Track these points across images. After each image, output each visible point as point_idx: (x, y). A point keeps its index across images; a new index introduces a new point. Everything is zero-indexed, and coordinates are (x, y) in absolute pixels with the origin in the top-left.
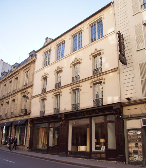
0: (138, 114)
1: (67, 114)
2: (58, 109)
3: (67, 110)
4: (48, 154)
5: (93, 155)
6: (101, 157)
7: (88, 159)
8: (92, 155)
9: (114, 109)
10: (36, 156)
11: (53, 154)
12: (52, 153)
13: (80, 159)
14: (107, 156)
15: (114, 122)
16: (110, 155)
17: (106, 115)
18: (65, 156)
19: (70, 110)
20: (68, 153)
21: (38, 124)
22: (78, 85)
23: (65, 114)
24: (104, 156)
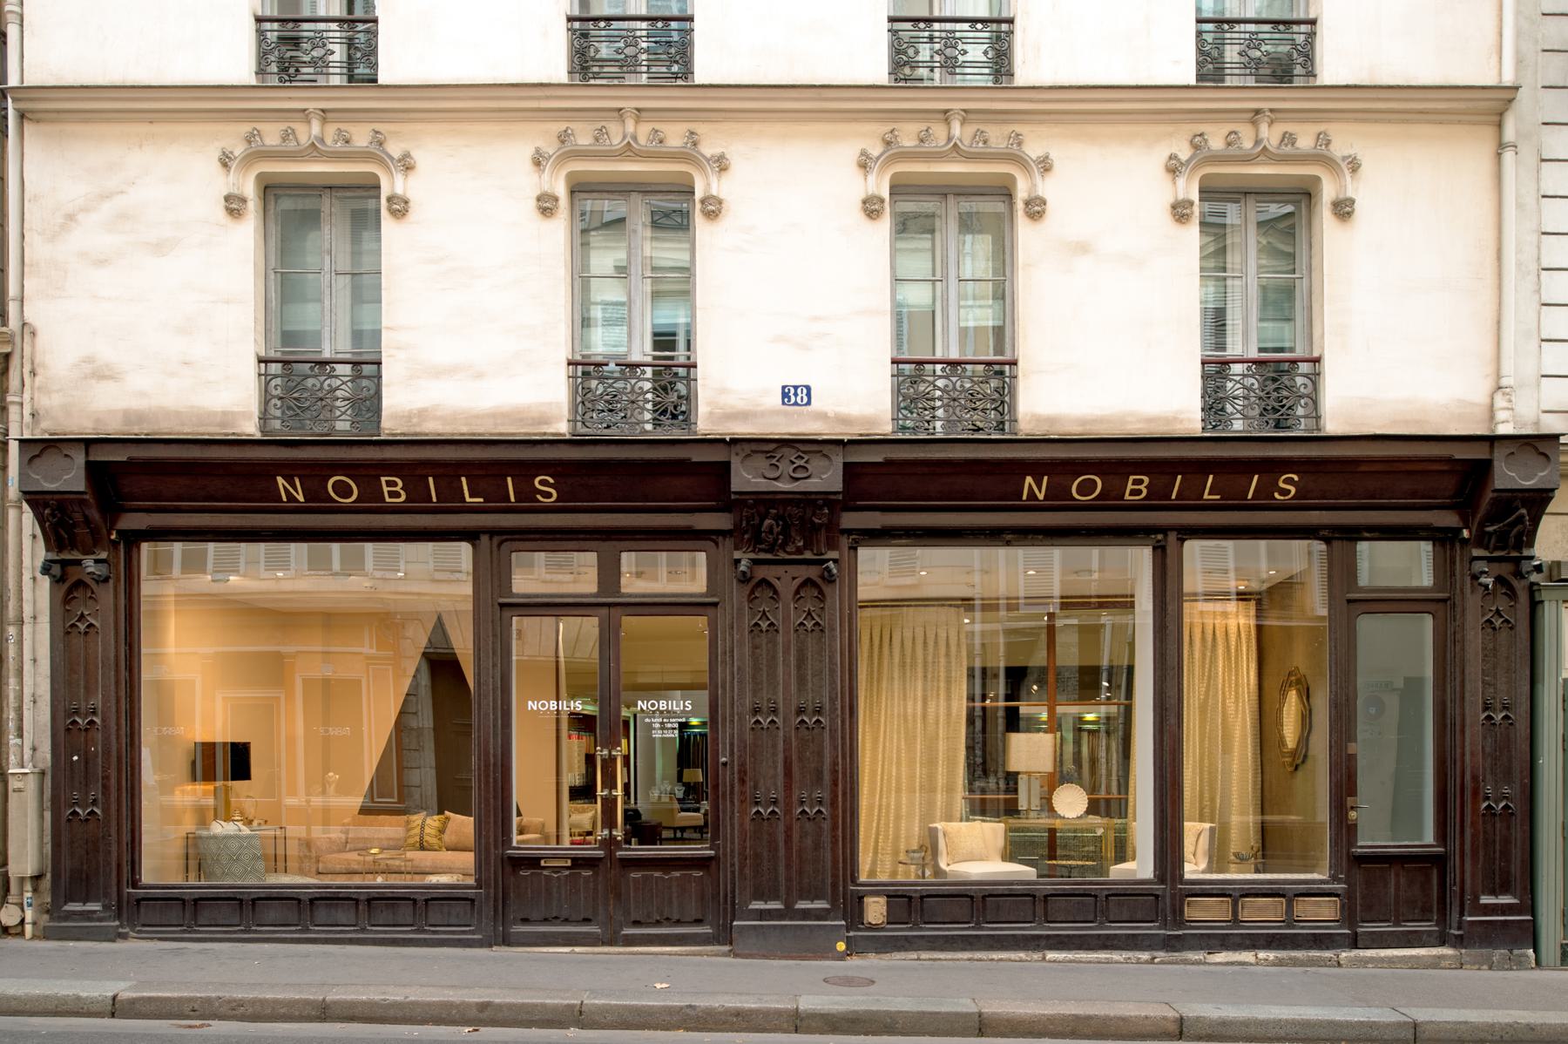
0: (1330, 577)
1: (889, 463)
2: (1285, 376)
3: (822, 416)
4: (507, 941)
5: (1202, 911)
6: (1290, 921)
7: (1161, 955)
8: (1189, 913)
9: (734, 488)
10: (670, 1010)
11: (612, 939)
12: (706, 930)
13: (1051, 955)
14: (1349, 916)
15: (1431, 607)
16: (639, 879)
17: (1343, 537)
18: (841, 946)
19: (871, 421)
20: (875, 910)
21: (1363, 547)
22: (997, 136)
23: (101, 455)
24: (1323, 911)
